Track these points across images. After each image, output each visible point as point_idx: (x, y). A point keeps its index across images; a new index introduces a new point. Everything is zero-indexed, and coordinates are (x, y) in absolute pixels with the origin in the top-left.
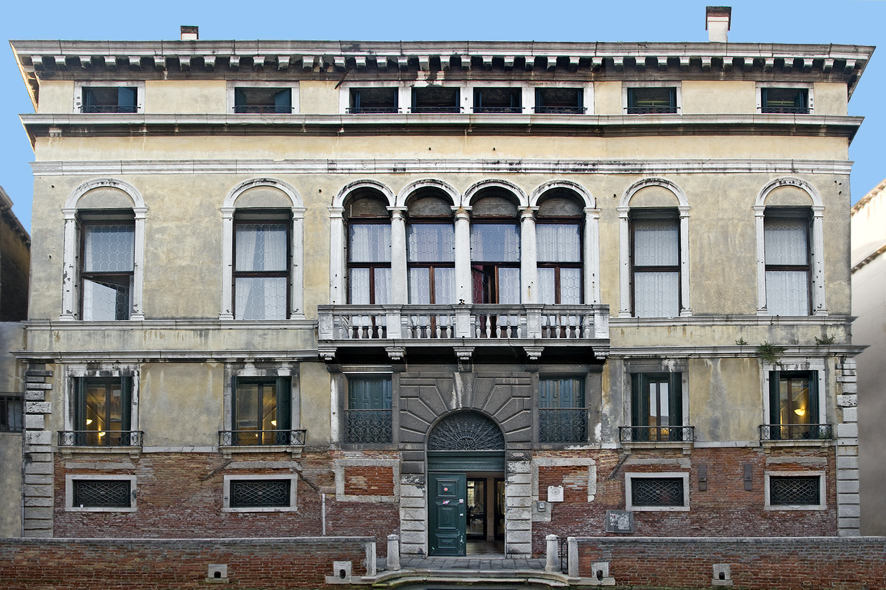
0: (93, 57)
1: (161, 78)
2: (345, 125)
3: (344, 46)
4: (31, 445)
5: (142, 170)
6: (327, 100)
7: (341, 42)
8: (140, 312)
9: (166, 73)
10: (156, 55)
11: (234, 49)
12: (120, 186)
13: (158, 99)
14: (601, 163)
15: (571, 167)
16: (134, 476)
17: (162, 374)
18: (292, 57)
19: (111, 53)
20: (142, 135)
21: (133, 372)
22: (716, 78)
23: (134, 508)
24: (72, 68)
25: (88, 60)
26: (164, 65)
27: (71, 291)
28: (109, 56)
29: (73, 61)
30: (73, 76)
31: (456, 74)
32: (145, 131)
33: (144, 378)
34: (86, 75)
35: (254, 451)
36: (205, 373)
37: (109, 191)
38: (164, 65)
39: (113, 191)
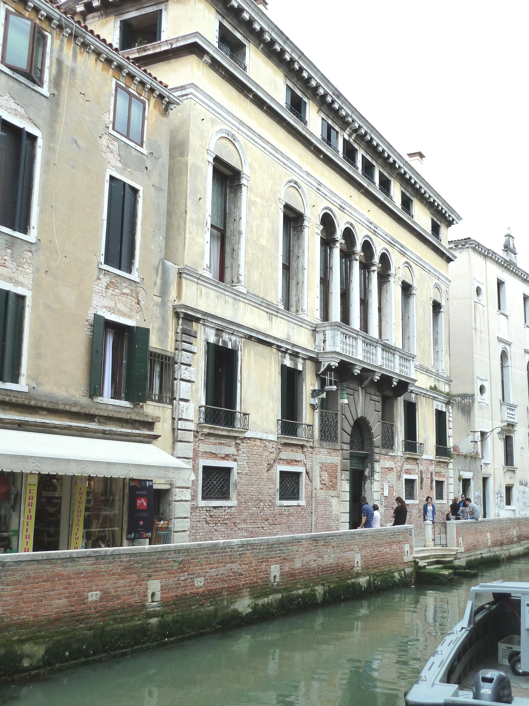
2: (326, 154)
3: (335, 92)
4: (180, 419)
7: (336, 89)
13: (259, 69)
14: (398, 243)
15: (389, 240)
19: (250, 11)
20: (247, 97)
23: (233, 502)
25: (236, 5)
30: (217, 6)
35: (220, 433)
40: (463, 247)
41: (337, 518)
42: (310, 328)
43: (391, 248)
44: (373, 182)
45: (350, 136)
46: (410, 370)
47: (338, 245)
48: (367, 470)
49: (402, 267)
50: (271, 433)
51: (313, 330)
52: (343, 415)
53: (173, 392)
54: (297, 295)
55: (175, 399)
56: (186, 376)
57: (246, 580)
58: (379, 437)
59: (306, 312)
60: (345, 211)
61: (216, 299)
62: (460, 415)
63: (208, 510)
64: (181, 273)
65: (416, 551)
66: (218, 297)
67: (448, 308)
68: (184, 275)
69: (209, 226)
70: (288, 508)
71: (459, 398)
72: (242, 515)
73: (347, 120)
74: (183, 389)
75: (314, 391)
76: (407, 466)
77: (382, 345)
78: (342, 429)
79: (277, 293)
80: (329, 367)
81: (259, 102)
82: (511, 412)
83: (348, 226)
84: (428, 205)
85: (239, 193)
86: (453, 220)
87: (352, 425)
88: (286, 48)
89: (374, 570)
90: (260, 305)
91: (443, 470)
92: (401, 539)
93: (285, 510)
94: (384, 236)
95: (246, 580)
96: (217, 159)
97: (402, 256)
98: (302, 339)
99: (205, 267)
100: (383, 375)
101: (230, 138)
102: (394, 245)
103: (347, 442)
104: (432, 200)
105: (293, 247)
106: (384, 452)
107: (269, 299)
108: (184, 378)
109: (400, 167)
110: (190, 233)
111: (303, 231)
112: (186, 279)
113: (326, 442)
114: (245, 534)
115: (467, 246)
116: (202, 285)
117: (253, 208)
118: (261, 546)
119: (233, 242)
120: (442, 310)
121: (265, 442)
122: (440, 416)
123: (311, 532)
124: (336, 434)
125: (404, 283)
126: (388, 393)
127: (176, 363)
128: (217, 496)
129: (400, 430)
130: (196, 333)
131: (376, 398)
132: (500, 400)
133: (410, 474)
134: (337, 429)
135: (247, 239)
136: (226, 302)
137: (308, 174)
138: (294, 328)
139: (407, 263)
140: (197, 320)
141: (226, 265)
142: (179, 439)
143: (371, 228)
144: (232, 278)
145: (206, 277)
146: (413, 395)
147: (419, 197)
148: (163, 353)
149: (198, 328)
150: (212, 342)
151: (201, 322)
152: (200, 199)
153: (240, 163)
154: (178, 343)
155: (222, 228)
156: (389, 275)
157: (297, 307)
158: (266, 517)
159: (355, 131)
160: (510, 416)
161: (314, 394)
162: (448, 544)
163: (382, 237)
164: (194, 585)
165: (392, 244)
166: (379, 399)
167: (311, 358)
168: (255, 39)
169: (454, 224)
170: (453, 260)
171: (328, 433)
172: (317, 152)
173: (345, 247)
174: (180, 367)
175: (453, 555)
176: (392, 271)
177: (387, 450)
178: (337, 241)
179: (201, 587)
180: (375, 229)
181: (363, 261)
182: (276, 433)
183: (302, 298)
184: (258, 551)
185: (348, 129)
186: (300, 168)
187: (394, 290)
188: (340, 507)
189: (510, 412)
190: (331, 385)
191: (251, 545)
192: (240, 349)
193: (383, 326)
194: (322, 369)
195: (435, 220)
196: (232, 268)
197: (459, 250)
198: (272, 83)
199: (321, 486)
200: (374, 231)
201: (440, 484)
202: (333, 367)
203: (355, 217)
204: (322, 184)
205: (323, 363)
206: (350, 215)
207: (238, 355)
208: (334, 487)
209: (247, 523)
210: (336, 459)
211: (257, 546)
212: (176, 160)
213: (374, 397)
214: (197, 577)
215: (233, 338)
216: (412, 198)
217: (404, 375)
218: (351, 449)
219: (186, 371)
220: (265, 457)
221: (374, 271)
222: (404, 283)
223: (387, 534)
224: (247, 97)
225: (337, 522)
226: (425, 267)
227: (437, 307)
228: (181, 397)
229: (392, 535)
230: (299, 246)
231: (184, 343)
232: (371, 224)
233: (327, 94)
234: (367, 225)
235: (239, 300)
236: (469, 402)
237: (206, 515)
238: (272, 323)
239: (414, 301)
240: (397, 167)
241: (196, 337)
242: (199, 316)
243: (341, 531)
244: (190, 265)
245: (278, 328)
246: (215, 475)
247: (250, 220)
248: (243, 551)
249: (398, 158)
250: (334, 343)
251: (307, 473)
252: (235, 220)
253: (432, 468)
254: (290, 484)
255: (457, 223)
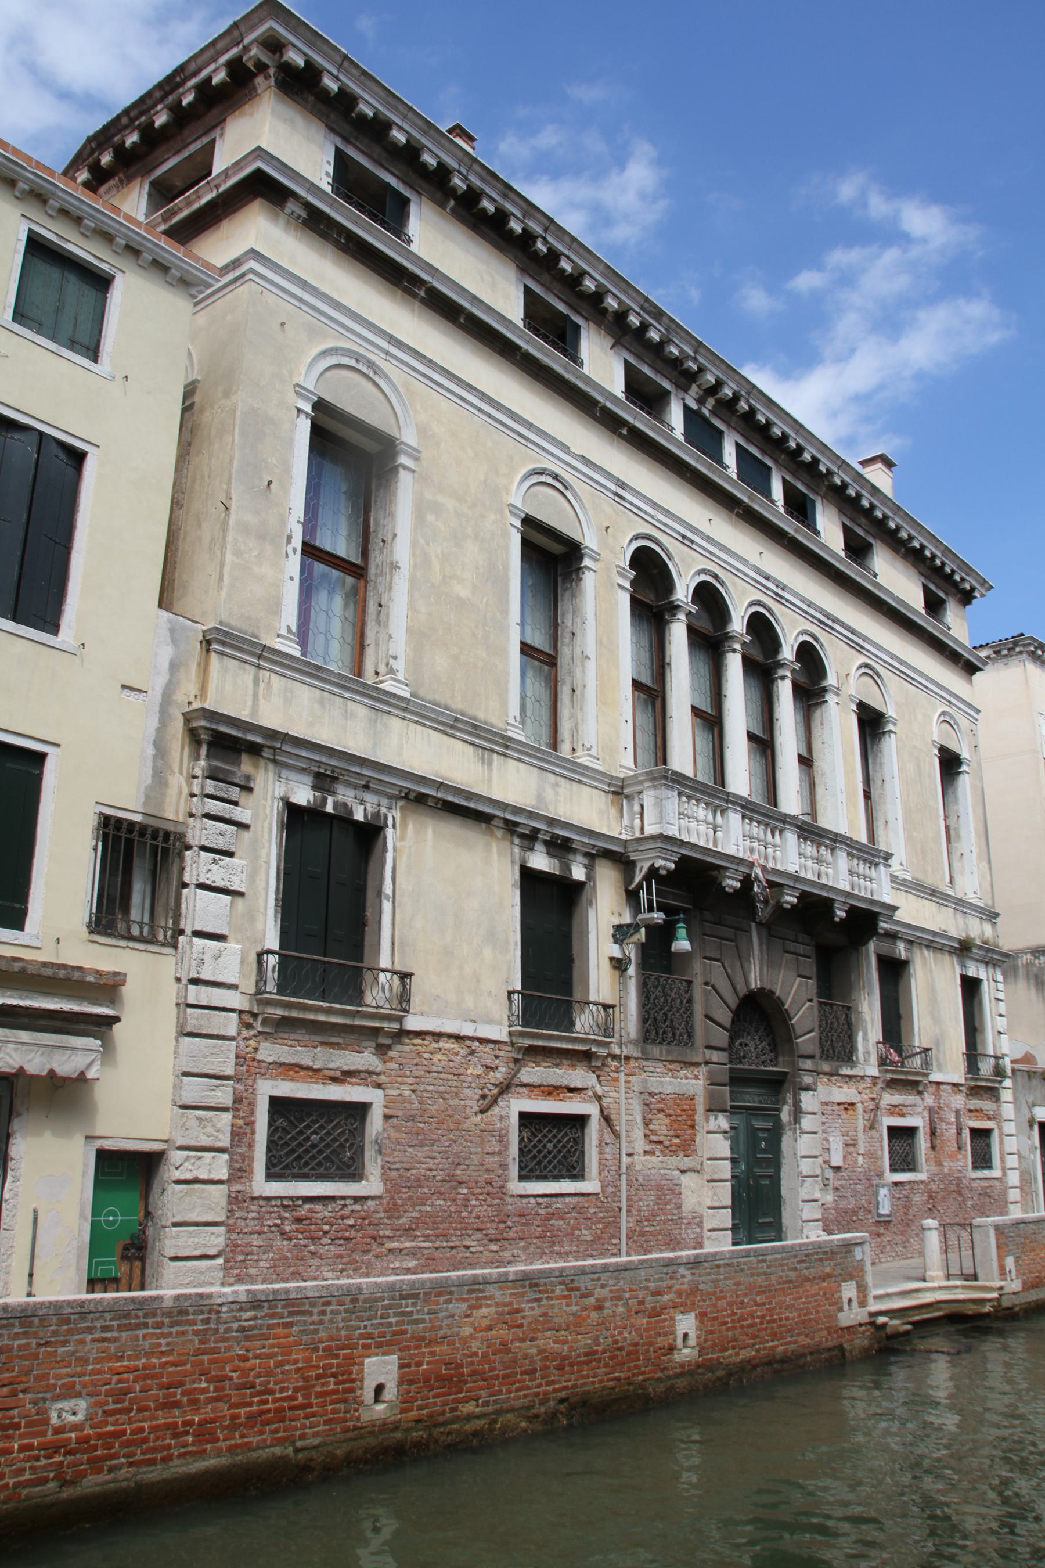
0: (308, 63)
1: (442, 205)
2: (634, 426)
3: (646, 305)
6: (602, 365)
9: (452, 203)
10: (459, 172)
11: (546, 230)
16: (380, 1092)
18: (599, 285)
20: (414, 295)
28: (400, 128)
29: (345, 101)
32: (422, 293)
33: (402, 838)
40: (1012, 652)
41: (696, 1220)
42: (606, 788)
43: (777, 604)
44: (773, 502)
45: (701, 401)
46: (880, 885)
50: (490, 1021)
51: (614, 793)
52: (706, 984)
53: (177, 917)
54: (572, 716)
55: (182, 932)
57: (266, 1402)
60: (694, 547)
62: (1033, 991)
63: (289, 1203)
64: (209, 642)
65: (876, 1297)
67: (979, 765)
68: (215, 646)
70: (545, 1199)
71: (1029, 956)
72: (399, 1217)
73: (685, 366)
75: (618, 928)
76: (890, 1098)
77: (798, 827)
78: (707, 1017)
83: (802, 638)
86: (973, 589)
87: (734, 1006)
89: (742, 1352)
90: (452, 727)
91: (987, 1105)
92: (828, 1270)
93: (539, 1204)
94: (805, 607)
95: (266, 1402)
96: (528, 521)
98: (585, 810)
100: (852, 907)
101: (364, 369)
103: (719, 1045)
105: (563, 615)
106: (826, 1067)
107: (481, 715)
108: (209, 882)
109: (830, 473)
110: (238, 553)
111: (581, 579)
112: (221, 654)
113: (677, 1048)
114: (411, 1264)
115: (1018, 649)
116: (271, 670)
117: (430, 517)
118: (329, 1303)
119: (381, 588)
121: (468, 1043)
123: (618, 1254)
125: (862, 707)
127: (189, 848)
131: (800, 949)
133: (903, 1115)
134: (691, 1016)
135: (413, 580)
137: (584, 459)
138: (557, 785)
139: (867, 666)
140: (255, 750)
141: (368, 641)
143: (767, 588)
144: (376, 665)
146: (901, 946)
148: (151, 822)
151: (264, 754)
153: (393, 421)
154: (195, 799)
157: (572, 742)
158: (478, 1224)
159: (713, 390)
161: (621, 933)
162: (980, 1275)
164: (46, 1421)
166: (809, 950)
167: (607, 855)
169: (975, 597)
171: (664, 1027)
172: (609, 422)
173: (802, 679)
174: (198, 855)
175: (990, 1300)
176: (831, 680)
177: (835, 1064)
178: (678, 606)
179: (75, 1427)
181: (802, 679)
182: (507, 1023)
183: (582, 720)
184: (315, 1318)
186: (565, 448)
187: (838, 723)
188: (706, 1194)
190: (651, 909)
191: (289, 1302)
194: (638, 878)
196: (377, 644)
197: (1004, 660)
199: (648, 1148)
200: (777, 594)
202: (663, 872)
204: (628, 485)
205: (639, 865)
206: (710, 556)
208: (687, 1147)
209: (416, 1237)
210: (693, 1083)
211: (313, 1305)
212: (216, 407)
213: (791, 946)
214: (57, 1398)
215: (370, 798)
216: (871, 540)
218: (731, 1062)
219: (214, 867)
220: (470, 1079)
222: (862, 707)
223: (783, 1259)
224: (410, 293)
225: (698, 1230)
227: (950, 764)
228: (198, 928)
229: (799, 1262)
230: (574, 612)
231: (207, 800)
232: (767, 578)
233: (628, 311)
235: (389, 713)
237: (280, 1217)
238: (490, 769)
239: (890, 746)
240: (824, 471)
241: (250, 790)
242: (258, 740)
243: (709, 1249)
244: (233, 623)
246: (316, 1122)
247: (422, 541)
248: (255, 1318)
249: (822, 453)
250: (661, 817)
251: (607, 1119)
252: (384, 541)
253: (959, 1101)
254: (553, 1143)
255: (982, 595)
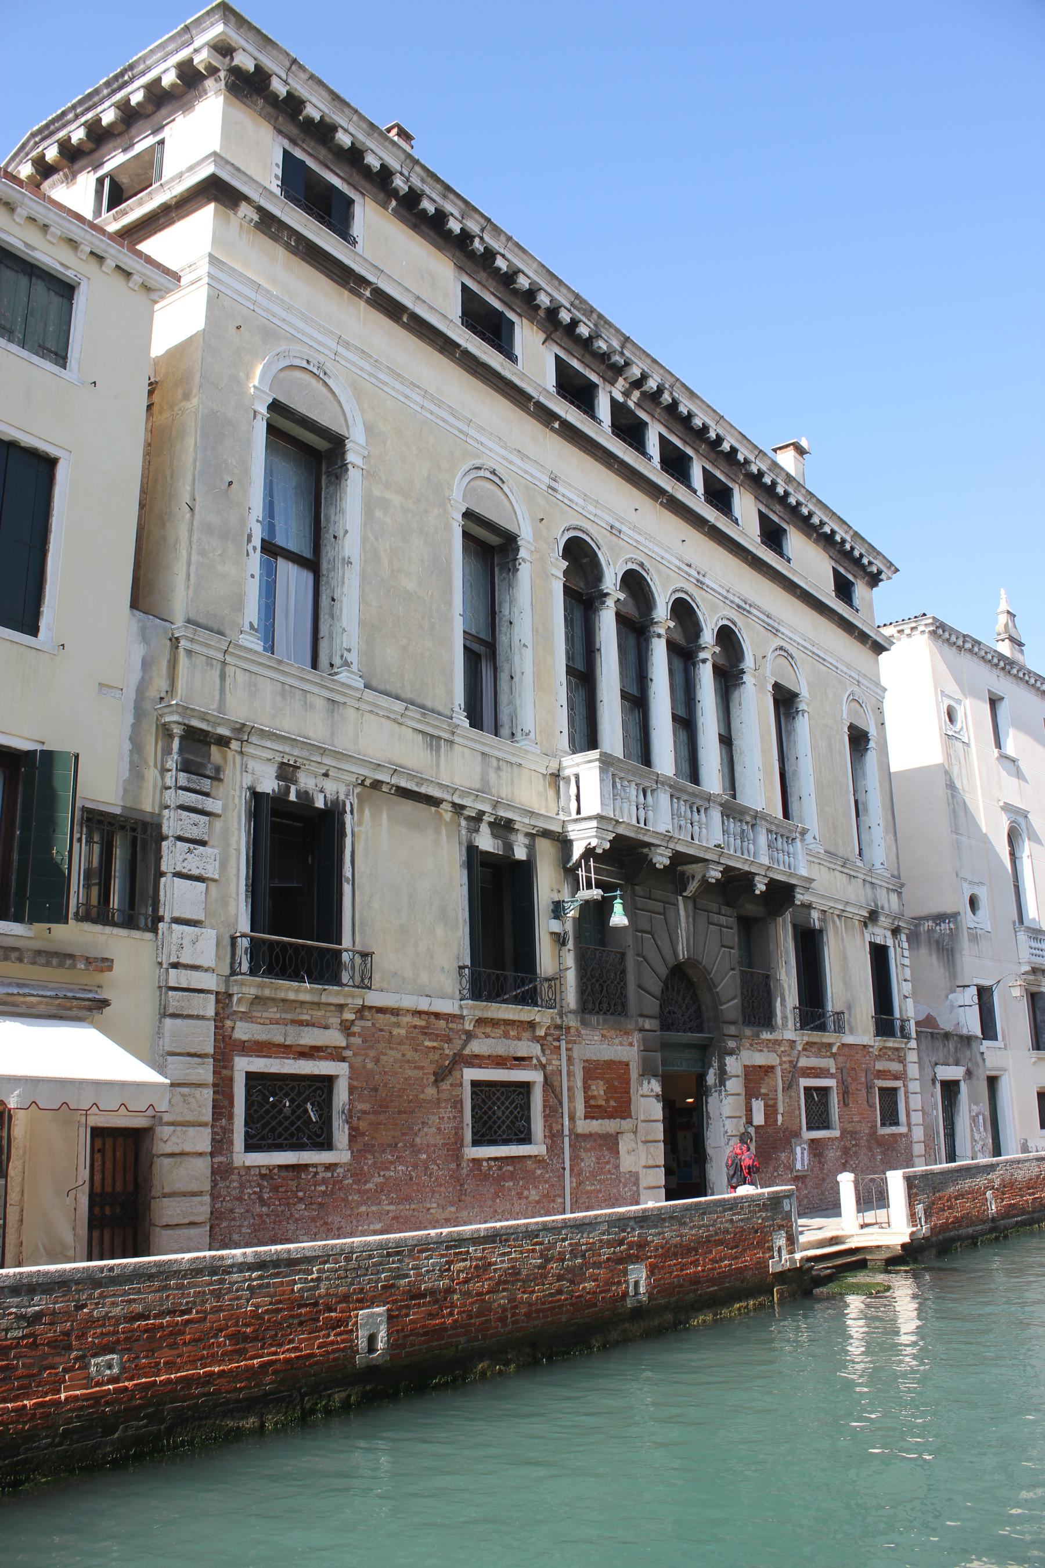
1: (385, 206)
3: (577, 302)
5: (362, 369)
7: (577, 296)
8: (355, 668)
12: (330, 382)
13: (377, 238)
14: (758, 608)
15: (737, 601)
17: (384, 816)
19: (352, 130)
20: (360, 296)
21: (344, 805)
22: (808, 536)
24: (287, 111)
25: (317, 117)
26: (401, 193)
27: (257, 577)
28: (346, 131)
31: (648, 405)
32: (368, 294)
34: (294, 131)
36: (438, 832)
37: (314, 382)
38: (401, 193)
39: (319, 386)
47: (610, 602)
48: (711, 1071)
49: (770, 656)
52: (638, 955)
54: (511, 702)
56: (193, 866)
58: (736, 1001)
59: (532, 735)
61: (278, 698)
63: (268, 1174)
66: (283, 694)
69: (257, 542)
71: (930, 923)
74: (177, 897)
78: (640, 986)
79: (450, 692)
80: (589, 852)
81: (389, 307)
82: (1038, 945)
84: (823, 542)
85: (343, 481)
88: (448, 207)
97: (769, 634)
99: (247, 628)
101: (315, 370)
102: (749, 612)
103: (650, 1013)
104: (874, 569)
105: (500, 605)
106: (748, 1032)
108: (185, 871)
109: (747, 462)
117: (378, 513)
120: (872, 744)
122: (879, 955)
124: (623, 995)
126: (752, 909)
128: (504, 1137)
129: (786, 986)
130: (218, 769)
131: (723, 920)
132: (1014, 923)
135: (364, 576)
136: (307, 706)
141: (321, 634)
142: (171, 1011)
145: (245, 648)
147: (800, 524)
149: (225, 758)
150: (268, 790)
152: (230, 483)
155: (490, 640)
156: (742, 672)
159: (638, 383)
160: (1037, 952)
163: (719, 594)
165: (744, 609)
168: (375, 190)
169: (882, 580)
170: (886, 649)
176: (748, 663)
180: (701, 578)
181: (721, 661)
182: (458, 996)
185: (621, 380)
189: (1034, 944)
190: (589, 886)
192: (348, 808)
193: (737, 775)
195: (842, 570)
196: (331, 637)
198: (435, 284)
201: (889, 1096)
203: (650, 550)
207: (343, 824)
208: (622, 1109)
210: (625, 1049)
212: (176, 409)
216: (785, 526)
217: (781, 867)
218: (662, 1029)
219: (189, 856)
221: (704, 661)
226: (824, 660)
228: (176, 914)
230: (511, 602)
232: (690, 566)
234: (679, 568)
236: (951, 929)
240: (742, 461)
245: (461, 767)
252: (335, 537)
255: (889, 578)
